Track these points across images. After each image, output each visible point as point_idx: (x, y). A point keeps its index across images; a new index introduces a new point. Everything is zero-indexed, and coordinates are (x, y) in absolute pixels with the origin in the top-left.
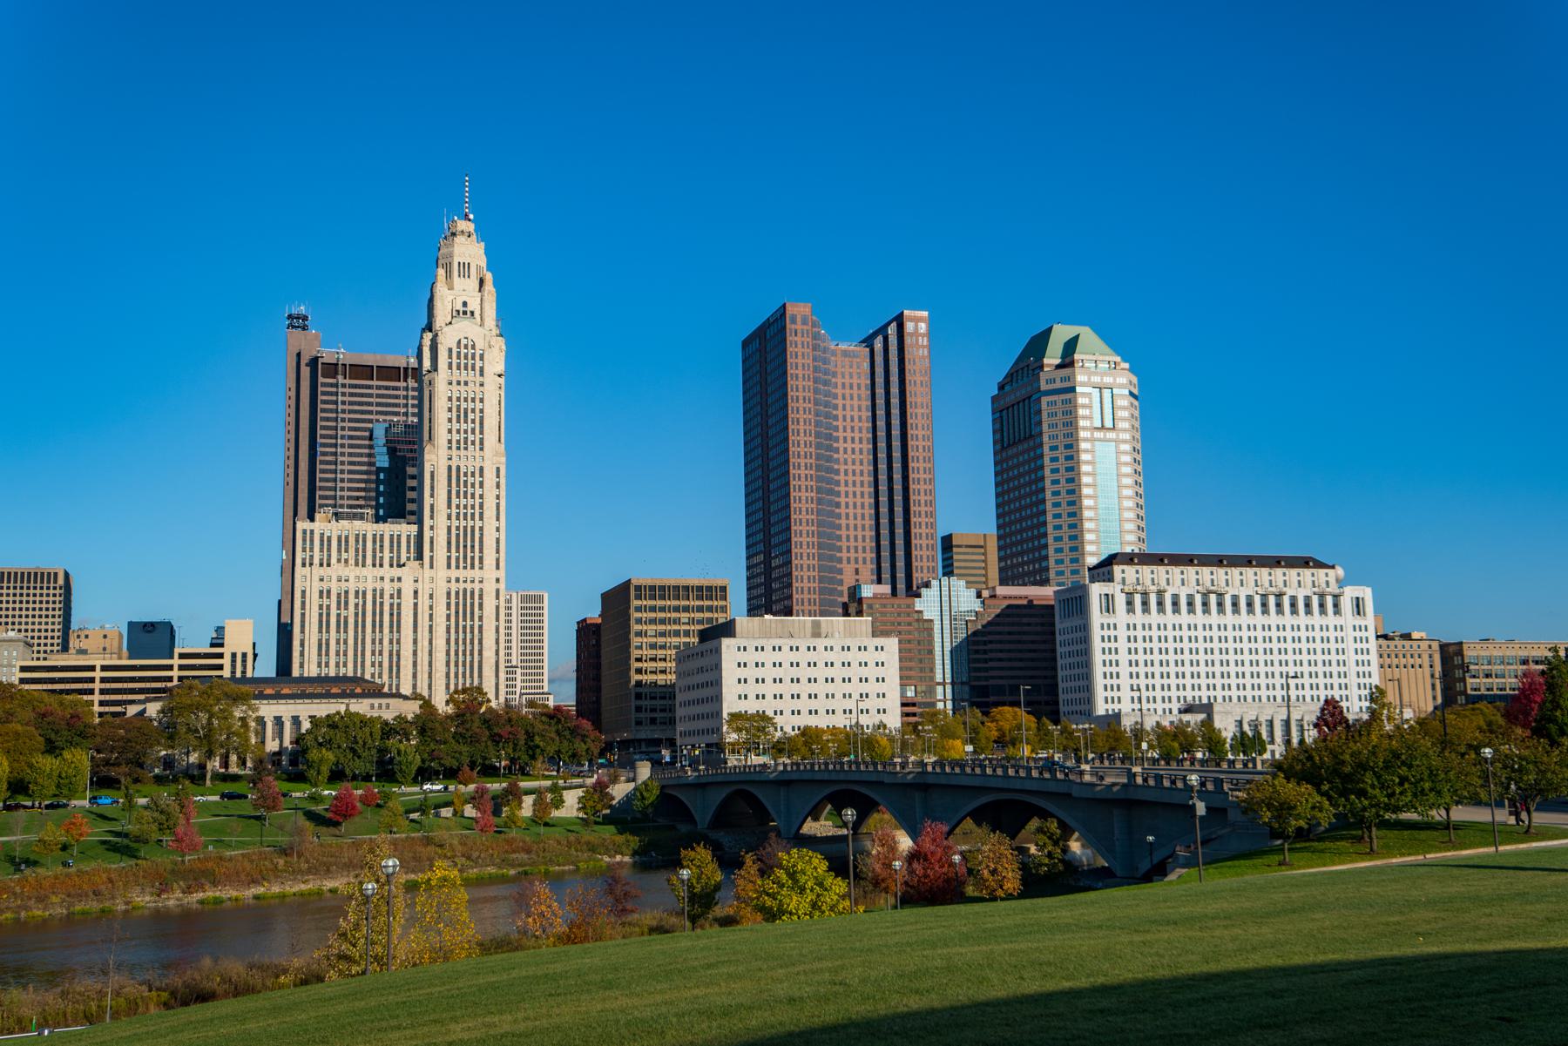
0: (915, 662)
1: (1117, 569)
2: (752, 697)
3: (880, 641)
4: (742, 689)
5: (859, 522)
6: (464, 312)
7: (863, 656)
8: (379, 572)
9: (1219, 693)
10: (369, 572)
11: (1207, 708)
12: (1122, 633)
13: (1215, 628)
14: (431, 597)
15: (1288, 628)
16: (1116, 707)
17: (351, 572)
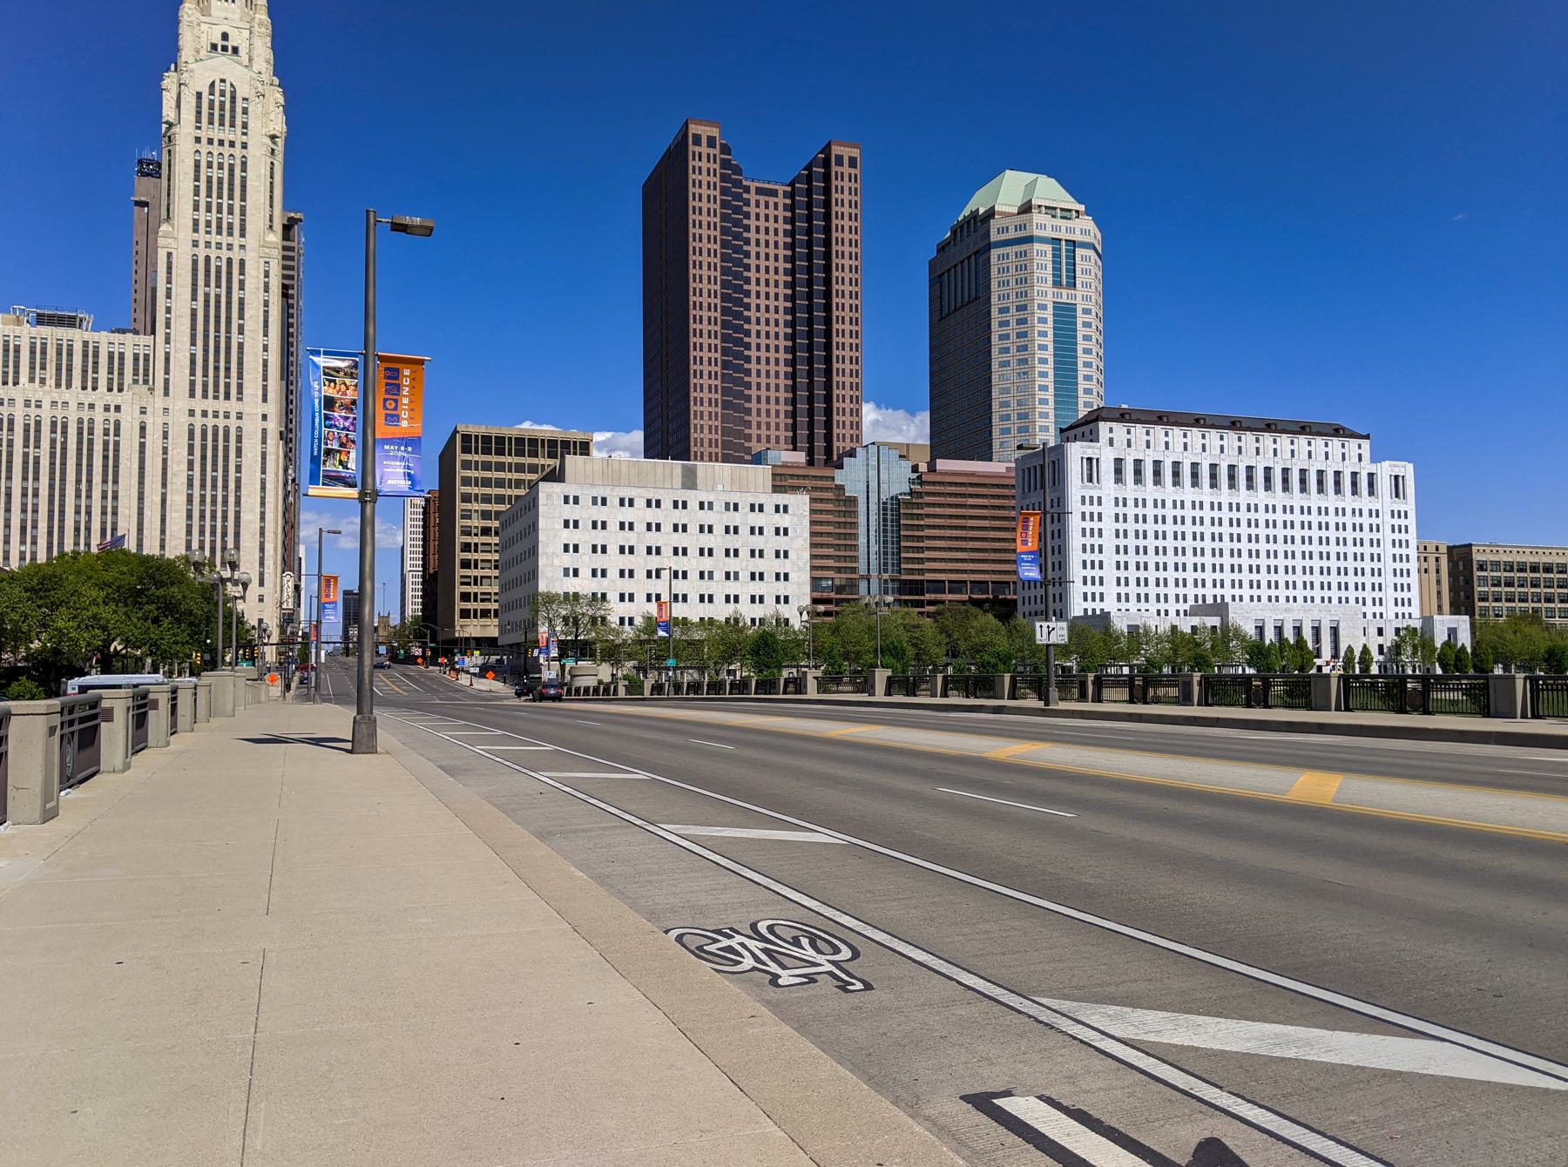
0: (833, 523)
1: (1103, 427)
2: (585, 572)
3: (782, 499)
4: (569, 560)
5: (772, 394)
6: (223, 46)
7: (757, 519)
8: (89, 396)
9: (1228, 592)
10: (74, 395)
11: (1220, 608)
12: (1108, 510)
13: (1225, 507)
14: (165, 436)
15: (1314, 511)
16: (1098, 606)
17: (47, 393)
